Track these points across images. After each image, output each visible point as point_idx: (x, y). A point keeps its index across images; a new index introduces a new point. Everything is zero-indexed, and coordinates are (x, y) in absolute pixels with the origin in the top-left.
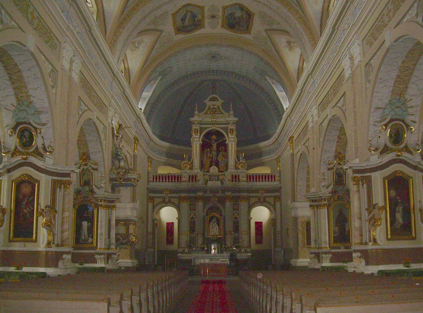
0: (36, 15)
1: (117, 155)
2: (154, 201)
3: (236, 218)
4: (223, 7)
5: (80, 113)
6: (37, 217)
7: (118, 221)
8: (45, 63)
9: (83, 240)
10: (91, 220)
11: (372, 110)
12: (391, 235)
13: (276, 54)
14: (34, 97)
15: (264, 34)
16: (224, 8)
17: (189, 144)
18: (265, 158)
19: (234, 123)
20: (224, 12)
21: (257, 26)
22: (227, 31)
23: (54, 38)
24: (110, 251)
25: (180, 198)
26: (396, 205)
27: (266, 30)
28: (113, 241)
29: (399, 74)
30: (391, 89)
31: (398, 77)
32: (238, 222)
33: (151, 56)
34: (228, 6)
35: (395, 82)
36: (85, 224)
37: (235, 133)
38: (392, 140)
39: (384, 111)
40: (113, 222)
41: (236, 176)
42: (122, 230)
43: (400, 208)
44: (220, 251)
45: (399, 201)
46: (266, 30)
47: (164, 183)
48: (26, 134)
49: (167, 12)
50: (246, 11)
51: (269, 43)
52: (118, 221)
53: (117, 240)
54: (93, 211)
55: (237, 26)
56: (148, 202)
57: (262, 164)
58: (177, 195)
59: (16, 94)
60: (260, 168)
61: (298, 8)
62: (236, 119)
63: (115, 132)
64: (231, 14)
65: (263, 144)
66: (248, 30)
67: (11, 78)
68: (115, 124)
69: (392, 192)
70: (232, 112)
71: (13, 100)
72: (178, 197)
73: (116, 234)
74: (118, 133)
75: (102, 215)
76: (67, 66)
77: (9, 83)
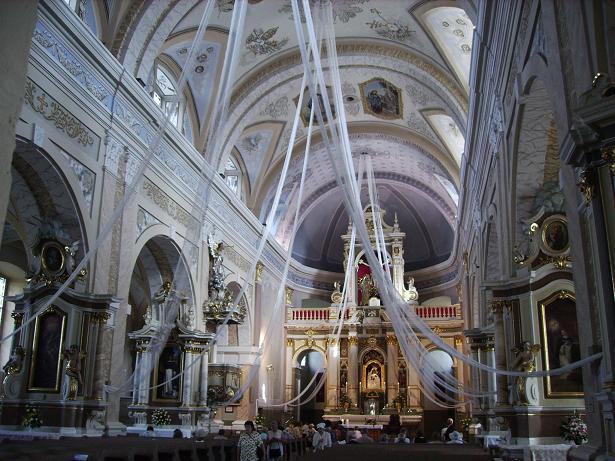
0: (48, 100)
1: (215, 283)
2: (294, 345)
3: (402, 367)
4: (359, 85)
5: (144, 227)
6: (62, 361)
7: (212, 369)
8: (70, 163)
9: (167, 393)
10: (177, 368)
11: (517, 201)
12: (552, 390)
13: (439, 142)
14: (59, 206)
15: (419, 115)
16: (362, 86)
17: (341, 270)
18: (443, 286)
19: (400, 240)
20: (362, 92)
21: (409, 105)
22: (253, 92)
23: (87, 130)
24: (200, 409)
25: (326, 341)
26: (561, 342)
27: (421, 111)
28: (205, 395)
29: (551, 143)
30: (543, 167)
31: (550, 147)
32: (405, 372)
33: (276, 156)
34: (365, 83)
35: (547, 156)
36: (169, 372)
37: (401, 252)
38: (551, 244)
39: (534, 201)
40: (206, 370)
41: (434, 310)
42: (217, 379)
43: (566, 348)
44: (379, 411)
45: (565, 337)
46: (421, 111)
47: (436, 318)
48: (54, 253)
49: (285, 98)
50: (391, 88)
51: (429, 129)
52: (212, 369)
53: (210, 394)
54: (179, 356)
55: (384, 109)
56: (286, 345)
57: (440, 294)
58: (323, 336)
59: (39, 204)
60: (439, 298)
61: (450, 76)
62: (403, 234)
63: (213, 254)
64: (372, 94)
65: (439, 266)
66: (398, 113)
67: (28, 184)
68: (214, 244)
69: (552, 323)
70: (396, 226)
71: (35, 211)
72: (454, 337)
73: (209, 387)
74: (216, 254)
75: (190, 358)
76: (113, 167)
77: (27, 188)
